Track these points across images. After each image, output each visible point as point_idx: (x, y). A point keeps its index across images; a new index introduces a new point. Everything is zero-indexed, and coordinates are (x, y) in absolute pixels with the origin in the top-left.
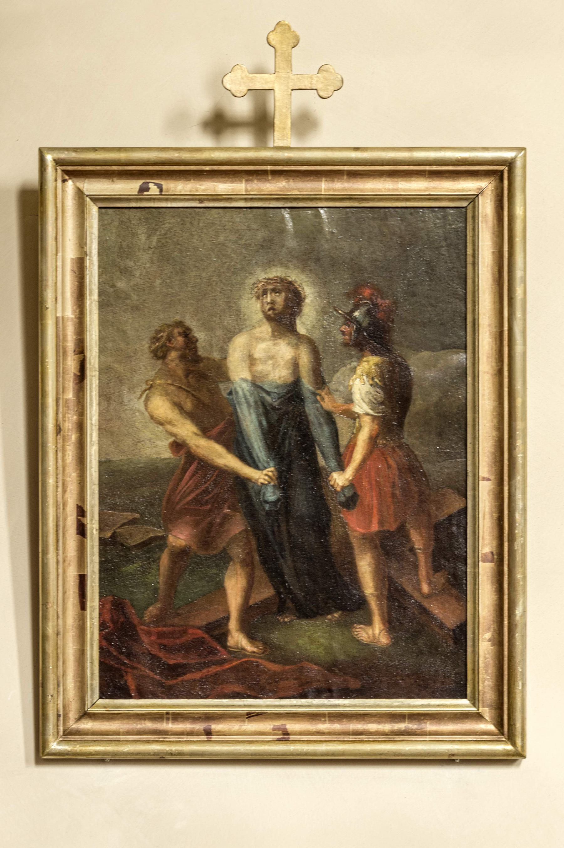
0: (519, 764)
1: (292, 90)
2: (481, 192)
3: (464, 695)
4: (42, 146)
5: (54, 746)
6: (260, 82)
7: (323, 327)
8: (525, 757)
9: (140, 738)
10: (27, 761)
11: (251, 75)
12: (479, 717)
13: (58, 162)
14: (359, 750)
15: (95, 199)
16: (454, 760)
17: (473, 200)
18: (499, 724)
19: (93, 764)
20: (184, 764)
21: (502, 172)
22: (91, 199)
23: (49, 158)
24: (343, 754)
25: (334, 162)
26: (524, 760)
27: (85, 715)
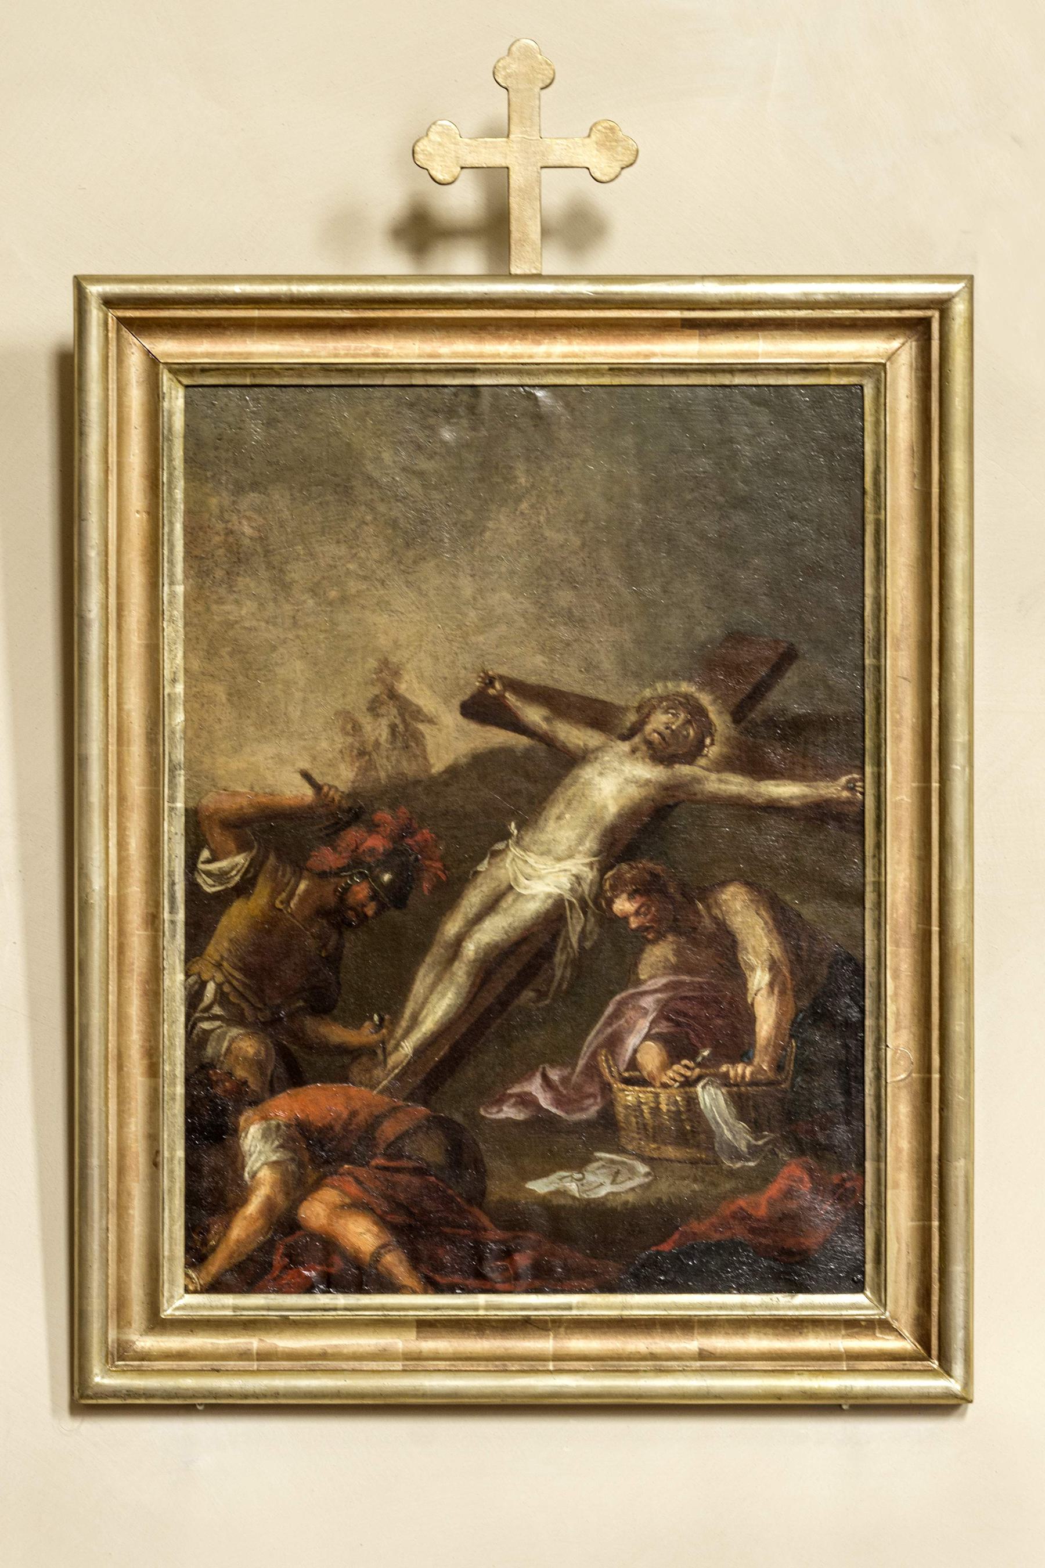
0: (963, 1415)
1: (542, 168)
2: (892, 356)
3: (859, 1287)
4: (80, 272)
5: (101, 1378)
6: (492, 154)
7: (231, 589)
8: (971, 1402)
9: (202, 1366)
10: (55, 1411)
11: (474, 143)
12: (884, 1326)
13: (109, 302)
14: (683, 1387)
15: (179, 370)
16: (194, 1405)
17: (877, 371)
18: (924, 1340)
19: (812, 1415)
20: (904, 1415)
21: (926, 322)
22: (170, 371)
23: (94, 290)
24: (338, 1394)
25: (704, 303)
26: (970, 1405)
27: (157, 1323)
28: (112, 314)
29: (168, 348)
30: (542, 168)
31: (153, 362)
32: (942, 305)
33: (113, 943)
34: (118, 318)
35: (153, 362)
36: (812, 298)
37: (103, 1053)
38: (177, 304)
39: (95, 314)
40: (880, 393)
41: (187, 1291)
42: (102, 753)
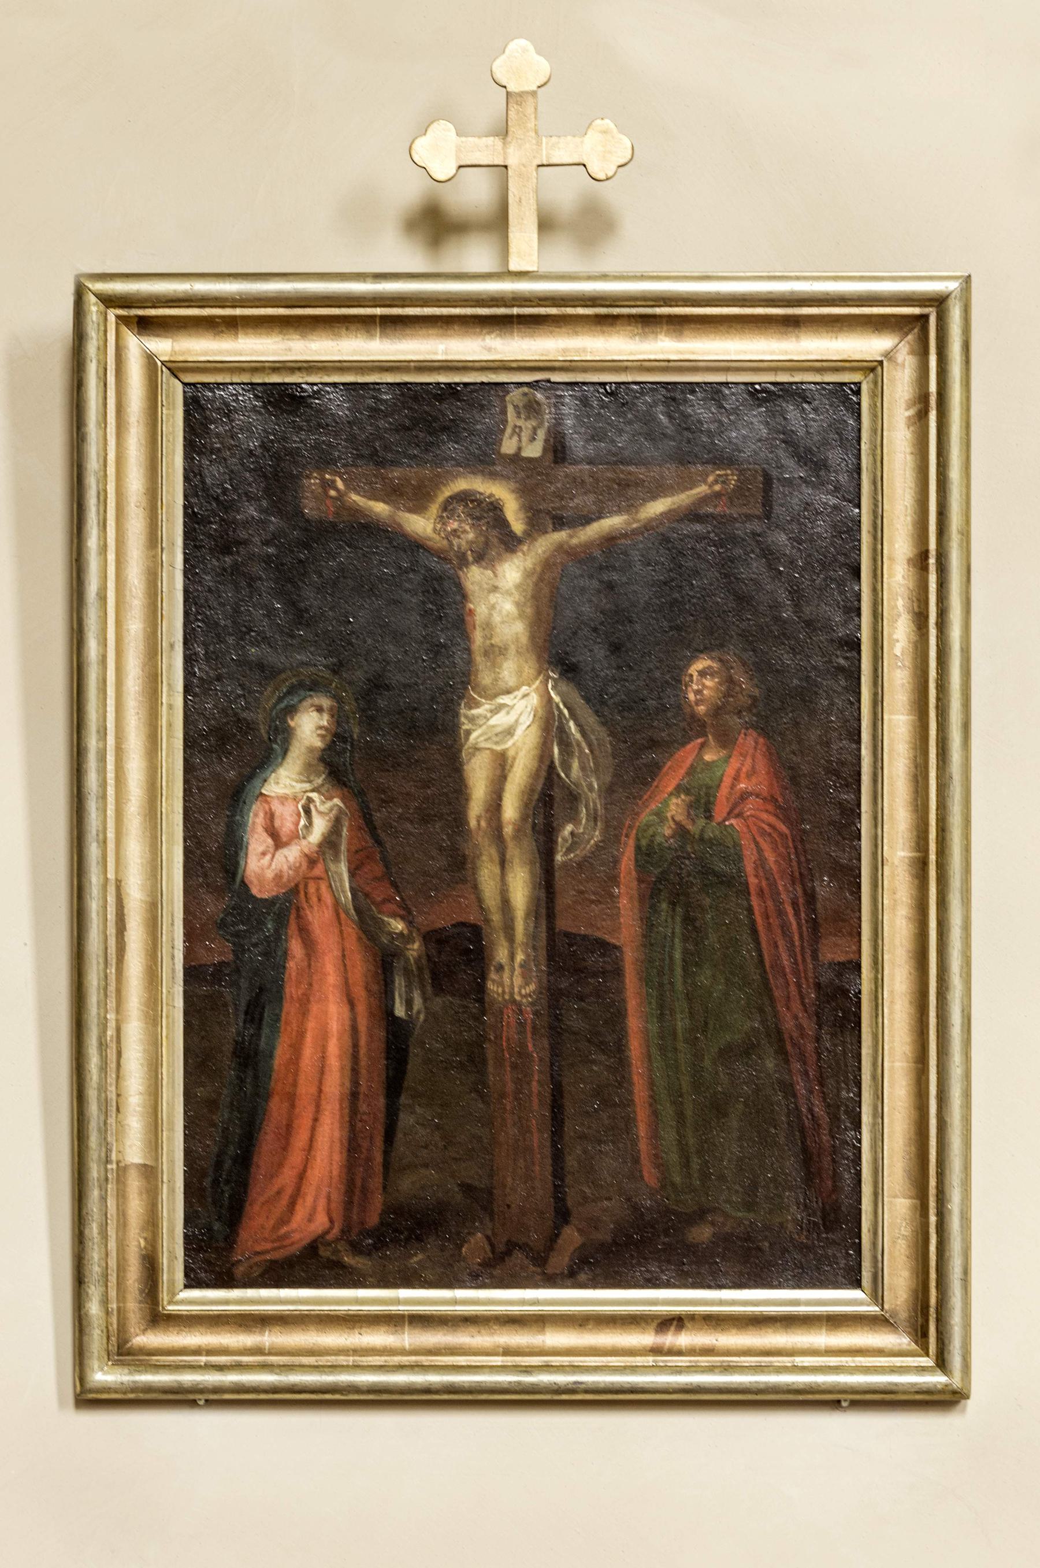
0: (963, 1411)
2: (888, 355)
3: (857, 1284)
15: (175, 369)
21: (925, 318)
28: (112, 314)
29: (163, 346)
30: (539, 166)
31: (150, 359)
32: (940, 302)
33: (111, 916)
34: (118, 317)
35: (150, 359)
36: (243, 1385)
37: (101, 939)
38: (155, 586)
39: (93, 306)
40: (878, 392)
41: (186, 1287)
42: (87, 1331)
